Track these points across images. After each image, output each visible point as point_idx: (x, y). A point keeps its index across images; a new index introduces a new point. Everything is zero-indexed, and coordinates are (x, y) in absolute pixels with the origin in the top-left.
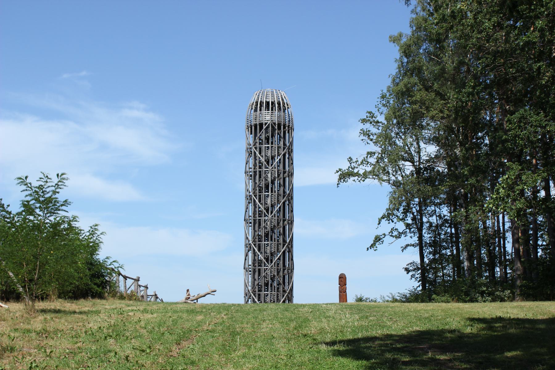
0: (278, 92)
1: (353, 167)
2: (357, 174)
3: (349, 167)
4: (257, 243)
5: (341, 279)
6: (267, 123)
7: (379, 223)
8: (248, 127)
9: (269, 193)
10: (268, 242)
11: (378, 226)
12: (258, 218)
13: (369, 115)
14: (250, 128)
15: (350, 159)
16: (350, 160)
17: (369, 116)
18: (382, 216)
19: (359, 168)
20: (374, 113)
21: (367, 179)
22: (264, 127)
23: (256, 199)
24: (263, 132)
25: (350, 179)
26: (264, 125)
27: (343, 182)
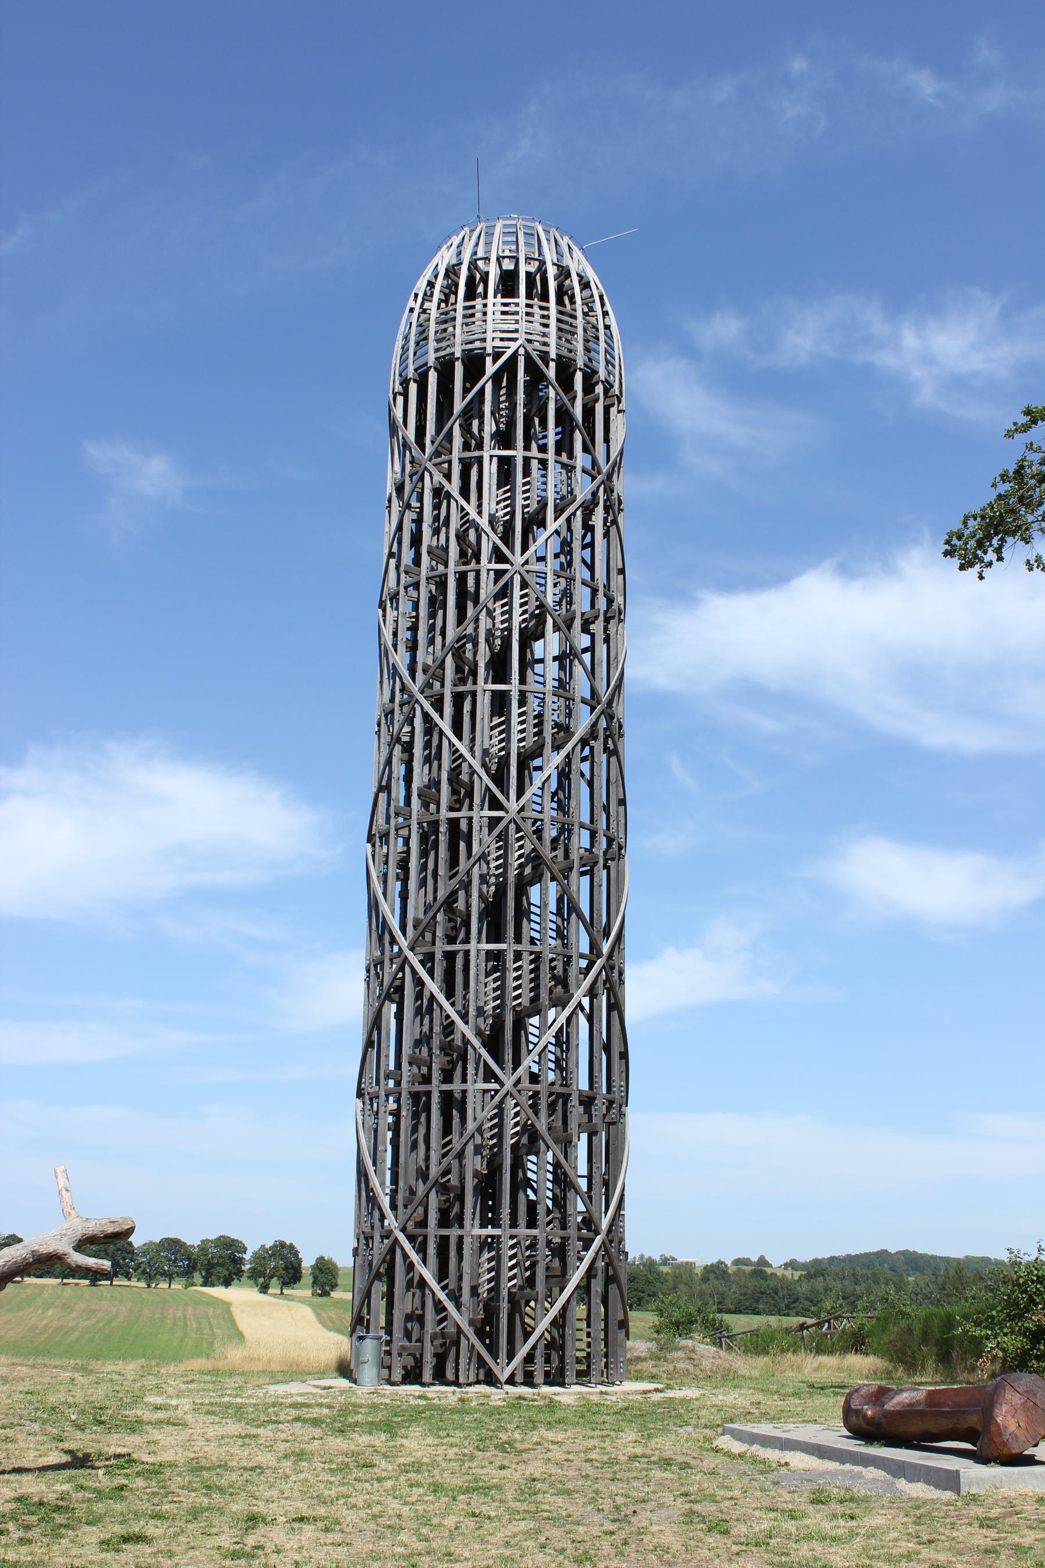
4: (440, 948)
12: (445, 814)
21: (978, 511)
22: (490, 368)
26: (489, 360)
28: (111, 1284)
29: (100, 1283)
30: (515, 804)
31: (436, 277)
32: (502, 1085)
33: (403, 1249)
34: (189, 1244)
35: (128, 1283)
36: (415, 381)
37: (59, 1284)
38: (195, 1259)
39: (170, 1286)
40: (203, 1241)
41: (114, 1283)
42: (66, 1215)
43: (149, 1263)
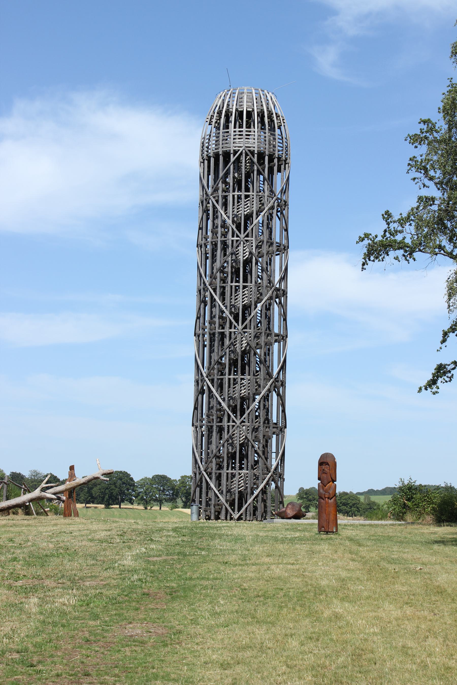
0: (261, 92)
1: (392, 230)
2: (401, 246)
3: (385, 231)
5: (323, 467)
6: (239, 150)
7: (444, 341)
8: (204, 160)
9: (243, 286)
10: (237, 377)
11: (441, 345)
12: (217, 330)
13: (425, 127)
14: (206, 162)
15: (387, 216)
16: (386, 216)
17: (425, 130)
18: (451, 327)
19: (405, 233)
20: (434, 122)
23: (216, 294)
24: (230, 167)
25: (388, 255)
26: (232, 155)
27: (374, 261)
28: (120, 507)
29: (112, 506)
30: (241, 327)
31: (214, 113)
32: (236, 423)
33: (205, 477)
34: (172, 479)
35: (131, 506)
36: (206, 160)
37: (84, 507)
38: (177, 489)
39: (160, 508)
40: (182, 477)
41: (122, 506)
42: (99, 469)
43: (145, 492)
